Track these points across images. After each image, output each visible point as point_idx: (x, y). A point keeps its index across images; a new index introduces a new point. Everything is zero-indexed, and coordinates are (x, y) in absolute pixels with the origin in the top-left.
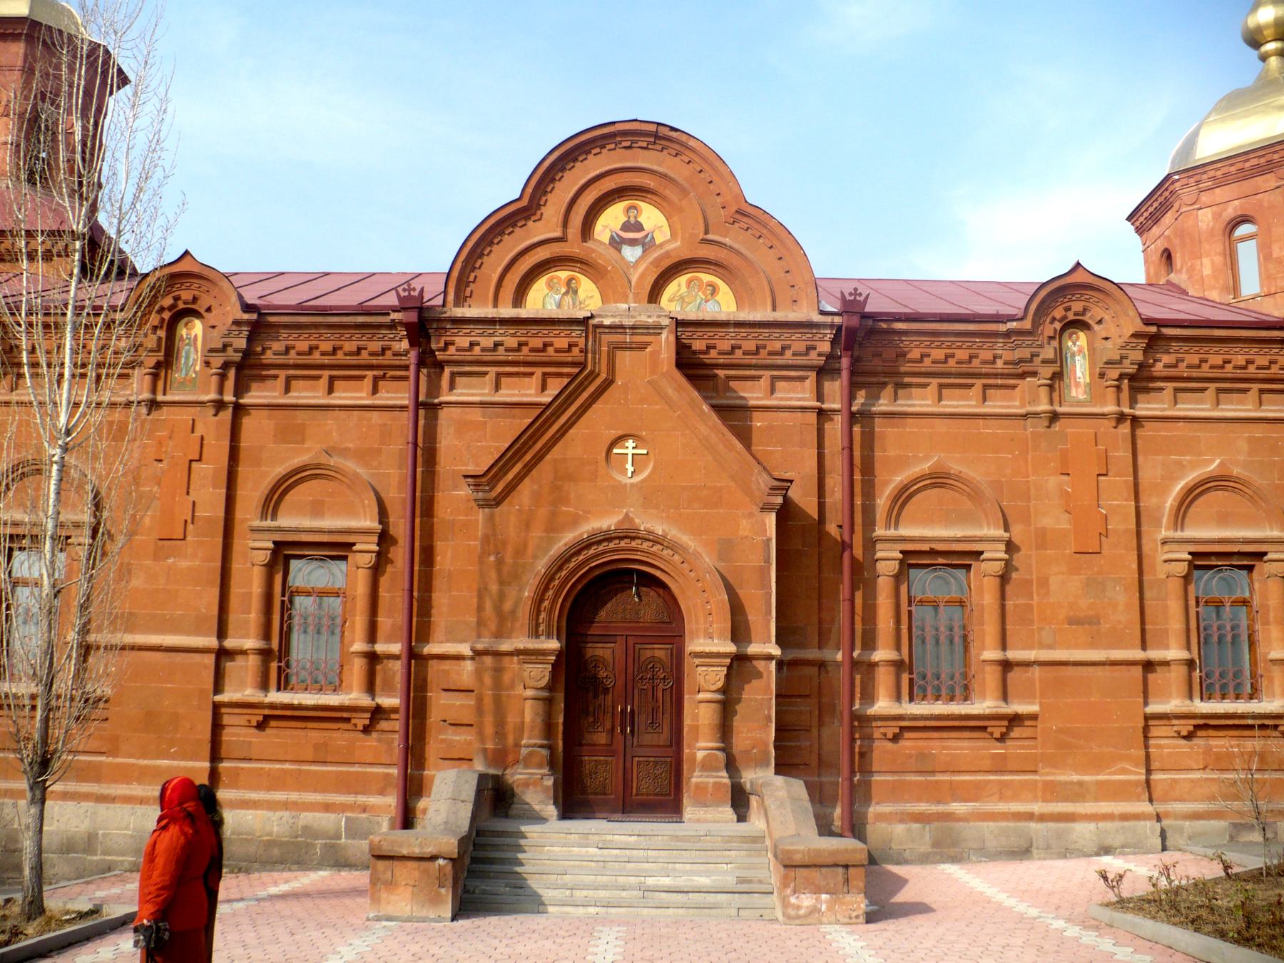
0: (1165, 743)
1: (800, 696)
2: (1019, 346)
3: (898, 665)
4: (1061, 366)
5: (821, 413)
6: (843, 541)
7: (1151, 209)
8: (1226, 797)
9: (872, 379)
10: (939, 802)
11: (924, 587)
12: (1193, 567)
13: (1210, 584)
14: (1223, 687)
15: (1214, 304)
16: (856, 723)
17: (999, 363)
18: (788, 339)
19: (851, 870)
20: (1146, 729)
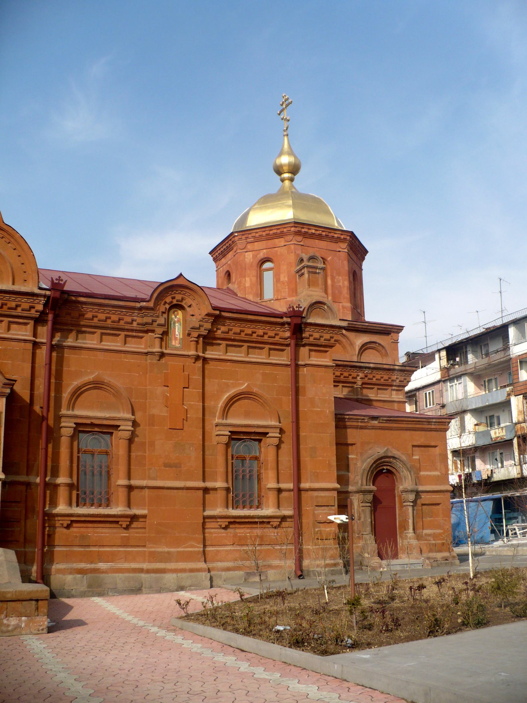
0: (214, 531)
1: (15, 502)
2: (146, 316)
3: (71, 486)
4: (168, 328)
5: (36, 345)
6: (43, 416)
7: (222, 249)
8: (242, 559)
9: (65, 327)
10: (92, 563)
11: (87, 444)
12: (231, 439)
13: (239, 448)
14: (244, 502)
15: (250, 302)
16: (46, 518)
17: (135, 324)
18: (20, 301)
19: (40, 603)
20: (204, 524)
